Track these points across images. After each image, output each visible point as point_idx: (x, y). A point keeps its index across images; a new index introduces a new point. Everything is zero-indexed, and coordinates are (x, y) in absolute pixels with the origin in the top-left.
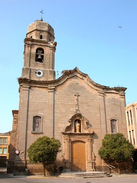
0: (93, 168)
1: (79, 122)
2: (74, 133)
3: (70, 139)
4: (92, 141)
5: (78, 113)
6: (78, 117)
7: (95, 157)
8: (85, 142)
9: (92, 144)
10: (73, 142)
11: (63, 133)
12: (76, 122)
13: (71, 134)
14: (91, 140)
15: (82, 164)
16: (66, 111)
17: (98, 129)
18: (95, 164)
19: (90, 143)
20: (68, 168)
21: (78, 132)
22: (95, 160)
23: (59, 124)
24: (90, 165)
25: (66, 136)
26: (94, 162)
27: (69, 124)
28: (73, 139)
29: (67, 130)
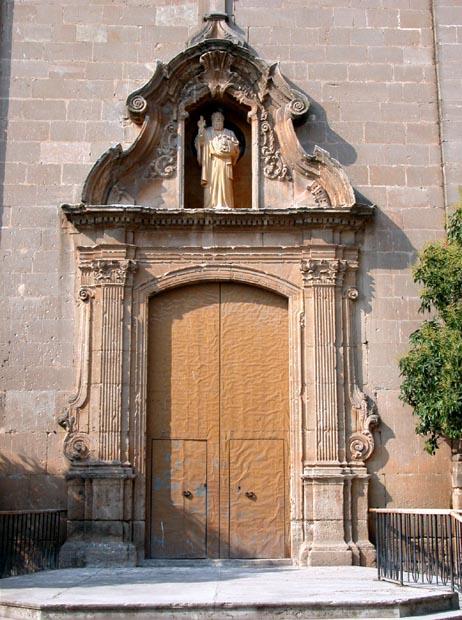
0: (350, 534)
1: (237, 120)
2: (229, 209)
3: (134, 271)
4: (349, 290)
5: (221, 36)
6: (217, 77)
7: (377, 427)
8: (283, 289)
9: (354, 315)
10: (164, 298)
11: (71, 215)
12: (202, 124)
13: (148, 225)
14: (343, 272)
15: (251, 496)
16: (114, 36)
17: (416, 177)
18: (377, 495)
19: (330, 305)
20: (107, 533)
21: (218, 201)
22: (375, 457)
23: (46, 145)
24: (329, 502)
25: (107, 239)
26: (372, 482)
27: (128, 136)
28: (164, 269)
29: (109, 189)
